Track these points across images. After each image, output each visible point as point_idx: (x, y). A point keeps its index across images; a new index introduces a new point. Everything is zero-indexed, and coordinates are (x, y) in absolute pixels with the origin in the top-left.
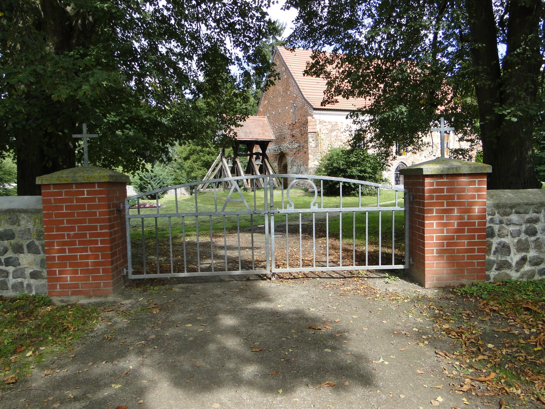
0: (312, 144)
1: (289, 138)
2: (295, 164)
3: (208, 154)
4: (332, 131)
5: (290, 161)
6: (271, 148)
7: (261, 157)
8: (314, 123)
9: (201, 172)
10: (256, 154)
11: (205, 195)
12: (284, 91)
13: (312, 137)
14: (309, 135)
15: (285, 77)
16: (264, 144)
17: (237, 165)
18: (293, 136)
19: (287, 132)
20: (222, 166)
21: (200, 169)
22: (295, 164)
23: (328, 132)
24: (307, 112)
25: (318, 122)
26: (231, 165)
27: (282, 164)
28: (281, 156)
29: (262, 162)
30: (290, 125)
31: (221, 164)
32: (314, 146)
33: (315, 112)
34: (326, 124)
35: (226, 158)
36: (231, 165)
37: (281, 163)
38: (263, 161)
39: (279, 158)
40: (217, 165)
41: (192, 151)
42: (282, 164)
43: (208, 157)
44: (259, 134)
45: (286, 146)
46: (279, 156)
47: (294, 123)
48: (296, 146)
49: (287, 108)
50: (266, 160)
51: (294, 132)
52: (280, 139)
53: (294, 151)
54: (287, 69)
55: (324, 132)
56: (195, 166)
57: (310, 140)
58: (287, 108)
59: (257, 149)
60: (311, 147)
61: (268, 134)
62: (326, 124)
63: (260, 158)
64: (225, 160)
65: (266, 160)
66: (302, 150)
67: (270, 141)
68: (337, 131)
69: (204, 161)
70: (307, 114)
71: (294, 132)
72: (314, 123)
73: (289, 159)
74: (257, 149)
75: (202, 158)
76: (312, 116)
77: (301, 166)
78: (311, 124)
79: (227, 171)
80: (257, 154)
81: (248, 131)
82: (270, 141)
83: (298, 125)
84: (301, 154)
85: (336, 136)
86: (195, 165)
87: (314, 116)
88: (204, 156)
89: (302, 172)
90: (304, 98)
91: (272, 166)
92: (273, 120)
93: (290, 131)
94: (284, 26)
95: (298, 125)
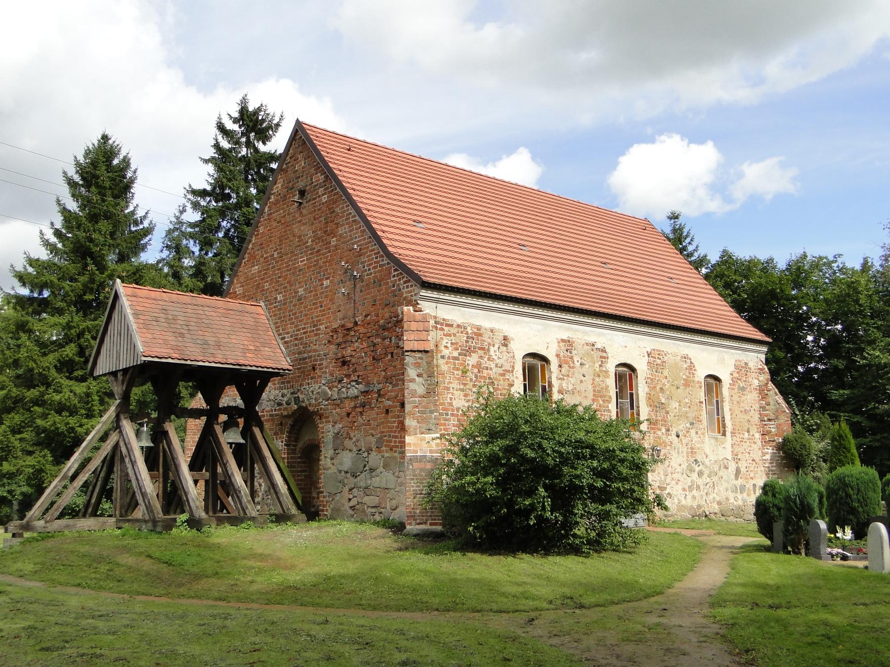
0: (415, 385)
1: (329, 368)
2: (348, 443)
3: (59, 412)
4: (467, 351)
5: (330, 435)
6: (271, 392)
7: (241, 421)
8: (421, 326)
9: (30, 460)
10: (228, 410)
11: (50, 544)
12: (316, 239)
13: (417, 365)
14: (409, 360)
15: (325, 198)
16: (252, 382)
17: (169, 444)
18: (344, 363)
19: (324, 351)
20: (116, 447)
21: (30, 453)
22: (348, 443)
23: (456, 354)
24: (397, 293)
25: (432, 322)
26: (147, 443)
27: (300, 445)
28: (301, 421)
29: (243, 435)
30: (335, 331)
31: (113, 438)
32: (421, 390)
33: (424, 293)
34: (453, 330)
35: (133, 419)
36: (147, 443)
37: (297, 440)
38: (246, 432)
39: (292, 426)
40: (104, 438)
41: (9, 403)
42: (300, 445)
43: (58, 418)
44: (245, 350)
45: (314, 392)
46: (290, 422)
47: (350, 325)
48: (353, 392)
49: (326, 283)
50: (256, 431)
51: (349, 351)
52: (305, 368)
53: (348, 405)
54: (330, 176)
55: (446, 352)
56: (17, 444)
57: (412, 373)
58: (326, 283)
59: (231, 397)
60: (414, 394)
61: (272, 355)
62: (453, 330)
63: (237, 425)
64: (128, 427)
65: (256, 431)
66: (382, 402)
67: (277, 375)
68: (481, 352)
69: (45, 430)
70: (397, 299)
71: (349, 351)
72: (421, 326)
73: (327, 431)
74: (231, 397)
75: (39, 422)
76: (415, 304)
77: (369, 450)
78: (414, 326)
79: (133, 463)
80: (231, 411)
81: (211, 340)
82: (277, 375)
83: (362, 330)
84: (370, 415)
85: (478, 366)
86: (15, 441)
87: (423, 304)
88: (44, 416)
89: (372, 470)
90: (389, 255)
91: (273, 447)
92: (281, 317)
93: (333, 347)
94: (275, 122)
95: (362, 330)
